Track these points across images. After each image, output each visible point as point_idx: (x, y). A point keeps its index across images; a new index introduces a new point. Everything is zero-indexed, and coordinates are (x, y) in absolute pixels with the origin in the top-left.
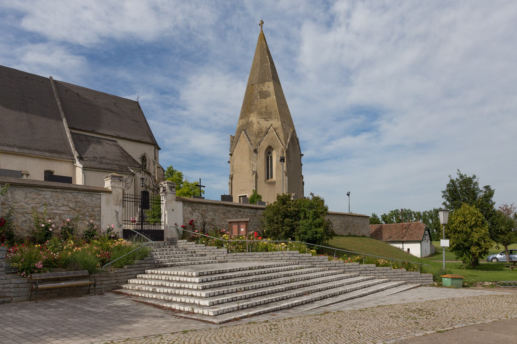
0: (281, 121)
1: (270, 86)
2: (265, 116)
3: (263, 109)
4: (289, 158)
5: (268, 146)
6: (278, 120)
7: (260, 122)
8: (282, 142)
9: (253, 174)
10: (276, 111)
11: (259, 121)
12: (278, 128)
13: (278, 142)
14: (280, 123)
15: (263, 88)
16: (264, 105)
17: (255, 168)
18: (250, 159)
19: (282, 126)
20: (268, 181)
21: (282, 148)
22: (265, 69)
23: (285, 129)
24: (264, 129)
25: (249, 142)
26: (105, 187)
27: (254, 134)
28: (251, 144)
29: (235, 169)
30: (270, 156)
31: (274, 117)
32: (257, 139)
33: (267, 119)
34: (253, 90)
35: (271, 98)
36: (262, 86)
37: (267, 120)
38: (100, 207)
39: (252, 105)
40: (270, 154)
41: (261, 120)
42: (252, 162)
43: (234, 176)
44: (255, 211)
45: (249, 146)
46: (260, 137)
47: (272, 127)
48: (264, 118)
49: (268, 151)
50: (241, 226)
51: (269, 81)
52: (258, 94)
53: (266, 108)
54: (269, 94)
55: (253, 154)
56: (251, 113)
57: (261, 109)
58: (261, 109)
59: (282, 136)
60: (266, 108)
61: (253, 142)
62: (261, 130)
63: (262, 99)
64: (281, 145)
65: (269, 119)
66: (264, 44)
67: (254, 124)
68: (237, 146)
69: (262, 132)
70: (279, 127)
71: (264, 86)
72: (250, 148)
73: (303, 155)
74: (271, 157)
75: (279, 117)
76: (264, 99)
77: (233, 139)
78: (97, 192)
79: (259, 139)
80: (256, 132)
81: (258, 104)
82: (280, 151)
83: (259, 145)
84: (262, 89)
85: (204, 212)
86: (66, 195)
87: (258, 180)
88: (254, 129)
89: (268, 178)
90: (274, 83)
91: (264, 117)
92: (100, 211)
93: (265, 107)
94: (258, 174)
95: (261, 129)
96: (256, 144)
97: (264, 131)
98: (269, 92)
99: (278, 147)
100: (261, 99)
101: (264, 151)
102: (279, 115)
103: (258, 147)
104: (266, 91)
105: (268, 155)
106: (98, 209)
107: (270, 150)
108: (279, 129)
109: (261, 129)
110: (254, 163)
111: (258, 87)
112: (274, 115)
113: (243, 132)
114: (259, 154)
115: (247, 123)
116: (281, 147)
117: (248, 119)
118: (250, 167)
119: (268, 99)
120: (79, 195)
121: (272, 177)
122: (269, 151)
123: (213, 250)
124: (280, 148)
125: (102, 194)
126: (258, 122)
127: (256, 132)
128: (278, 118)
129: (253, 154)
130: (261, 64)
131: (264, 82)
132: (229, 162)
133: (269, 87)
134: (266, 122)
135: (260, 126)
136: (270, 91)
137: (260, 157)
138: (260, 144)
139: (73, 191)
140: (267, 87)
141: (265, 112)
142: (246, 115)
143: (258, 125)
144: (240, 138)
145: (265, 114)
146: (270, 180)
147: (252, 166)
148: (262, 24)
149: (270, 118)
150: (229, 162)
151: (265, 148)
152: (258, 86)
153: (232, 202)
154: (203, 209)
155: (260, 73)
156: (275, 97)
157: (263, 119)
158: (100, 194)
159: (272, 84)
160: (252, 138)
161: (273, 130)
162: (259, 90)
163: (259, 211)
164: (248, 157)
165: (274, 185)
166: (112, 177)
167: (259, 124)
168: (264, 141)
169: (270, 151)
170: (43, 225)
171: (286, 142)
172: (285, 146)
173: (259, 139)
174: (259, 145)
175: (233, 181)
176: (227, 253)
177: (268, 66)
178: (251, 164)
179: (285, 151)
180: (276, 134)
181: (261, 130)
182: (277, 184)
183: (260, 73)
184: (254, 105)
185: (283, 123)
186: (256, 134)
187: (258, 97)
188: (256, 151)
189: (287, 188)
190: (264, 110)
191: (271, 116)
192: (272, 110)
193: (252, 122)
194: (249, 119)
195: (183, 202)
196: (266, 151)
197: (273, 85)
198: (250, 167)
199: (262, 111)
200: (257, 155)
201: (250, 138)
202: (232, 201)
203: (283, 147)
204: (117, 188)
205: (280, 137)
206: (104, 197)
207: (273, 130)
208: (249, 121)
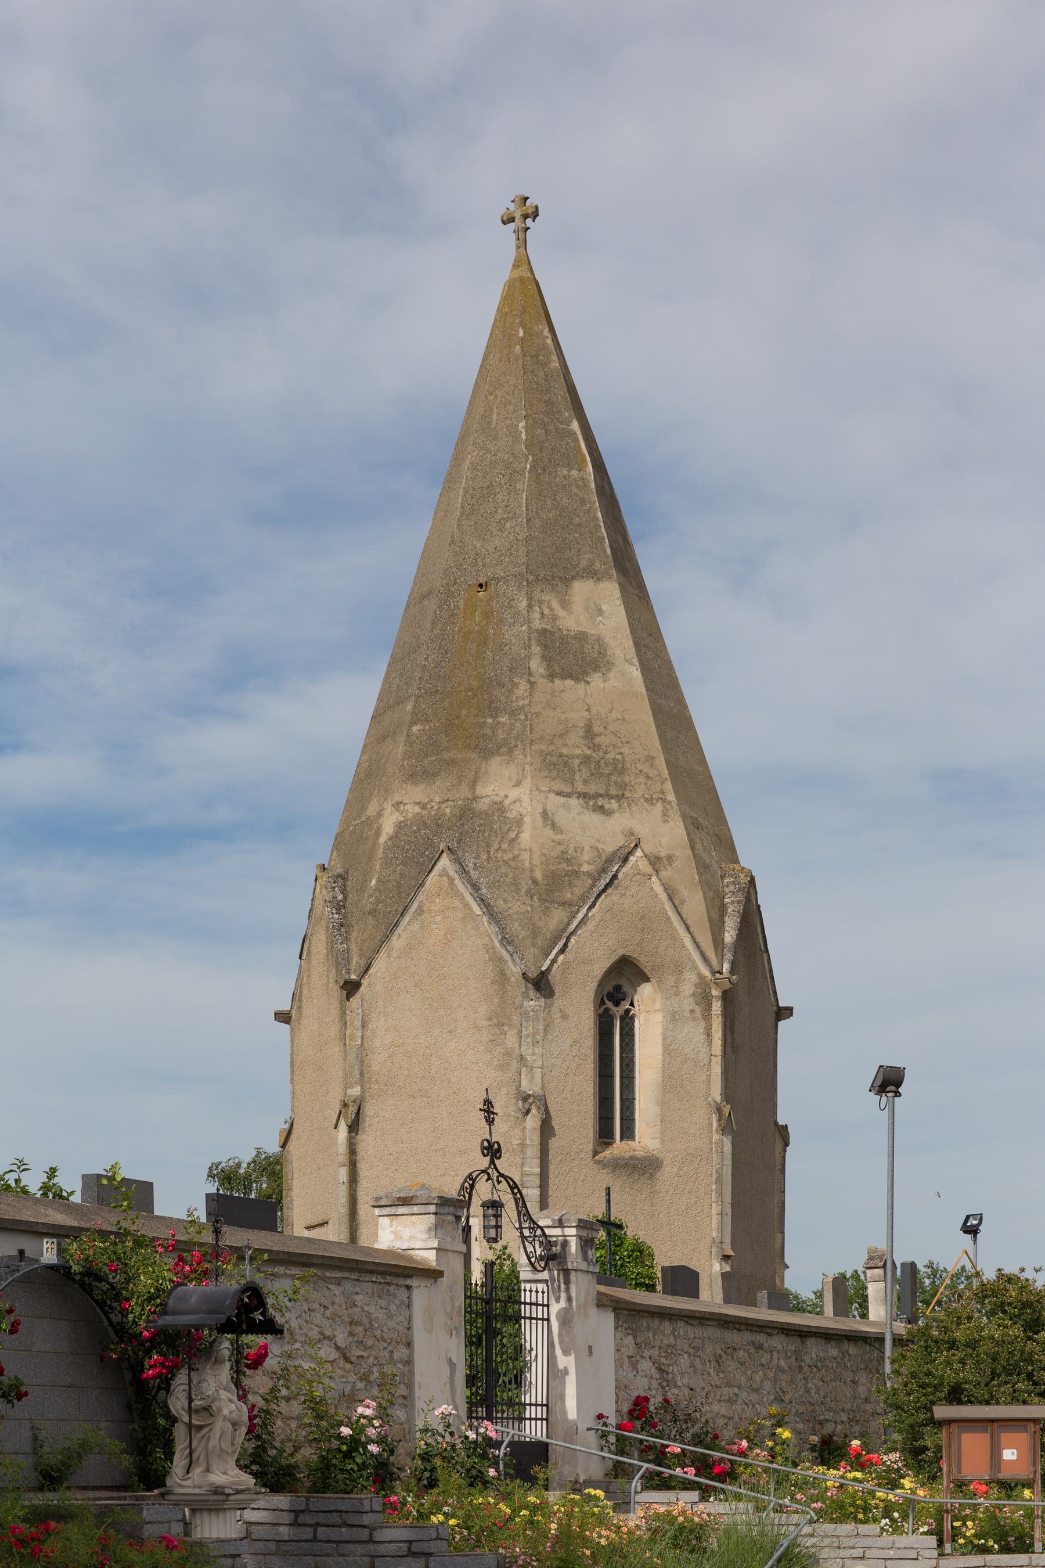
0: (683, 816)
1: (604, 607)
2: (585, 782)
3: (574, 738)
4: (732, 1033)
5: (614, 958)
6: (665, 813)
7: (562, 818)
8: (700, 939)
9: (528, 1112)
10: (651, 759)
11: (549, 807)
12: (670, 858)
13: (675, 938)
14: (683, 832)
15: (561, 613)
16: (578, 717)
17: (538, 1079)
18: (499, 1021)
19: (693, 849)
20: (607, 1153)
21: (701, 977)
22: (565, 502)
23: (707, 867)
24: (586, 856)
25: (492, 929)
26: (376, 1246)
27: (525, 883)
28: (506, 940)
29: (375, 1068)
30: (618, 1011)
31: (640, 790)
32: (546, 911)
33: (600, 802)
34: (487, 615)
35: (614, 680)
36: (555, 604)
37: (601, 809)
38: (409, 1345)
39: (494, 711)
40: (617, 1004)
41: (567, 808)
42: (511, 1041)
43: (369, 1110)
44: (792, 1344)
45: (489, 949)
46: (564, 904)
47: (639, 853)
48: (583, 795)
49: (609, 988)
50: (1005, 1437)
51: (592, 574)
52: (536, 649)
53: (589, 734)
54: (602, 653)
55: (525, 995)
56: (487, 754)
57: (558, 741)
58: (558, 741)
59: (695, 903)
60: (589, 734)
61: (516, 928)
62: (568, 861)
63: (558, 682)
64: (696, 956)
65: (614, 804)
66: (544, 344)
67: (519, 822)
68: (397, 942)
69: (576, 873)
70: (677, 853)
71: (565, 604)
72: (501, 959)
73: (788, 1012)
74: (628, 1020)
75: (671, 797)
76: (569, 682)
77: (344, 892)
78: (398, 1275)
79: (558, 916)
80: (538, 875)
81: (538, 709)
82: (688, 989)
83: (562, 951)
84: (555, 618)
85: (666, 1358)
86: (327, 1293)
87: (553, 1143)
88: (526, 856)
89: (604, 1135)
90: (623, 588)
91: (580, 787)
92: (409, 1362)
93: (581, 733)
94: (553, 1114)
95: (564, 857)
96: (539, 942)
97: (585, 868)
98: (599, 640)
99: (679, 969)
100: (551, 677)
101: (592, 986)
102: (668, 785)
103: (554, 961)
104: (582, 637)
105: (609, 1004)
106: (401, 1353)
107: (623, 982)
108: (676, 864)
109: (564, 857)
110: (526, 1050)
111: (530, 606)
112: (642, 779)
113: (445, 862)
114: (558, 1002)
115: (466, 812)
116: (695, 967)
117: (473, 785)
118: (502, 1067)
119: (596, 680)
120: (358, 1290)
121: (628, 1133)
122: (614, 983)
123: (861, 1542)
124: (690, 977)
125: (414, 1282)
126: (545, 815)
127: (538, 875)
128: (664, 801)
129: (525, 995)
130: (539, 469)
131: (567, 581)
132: (283, 1017)
133: (600, 612)
134: (595, 819)
135: (557, 837)
136: (608, 640)
137: (565, 1017)
138: (566, 945)
139: (346, 1275)
140: (587, 609)
141: (586, 760)
142: (453, 762)
143: (548, 832)
144: (421, 896)
145: (585, 773)
146: (619, 1147)
147: (515, 1065)
148: (525, 217)
149: (620, 798)
150: (283, 1017)
151: (601, 967)
152: (530, 599)
153: (697, 1297)
154: (666, 1342)
155: (537, 523)
156: (636, 673)
157: (574, 802)
158: (408, 1282)
159: (617, 594)
160: (514, 906)
161: (649, 869)
162: (538, 624)
163: (811, 1342)
164: (483, 1009)
165: (652, 1175)
166: (583, 1228)
167: (553, 825)
168: (590, 926)
169: (618, 988)
170: (346, 1431)
171: (718, 943)
172: (717, 968)
173: (558, 916)
174: (562, 951)
175: (367, 1142)
176: (935, 1553)
177: (586, 486)
178: (508, 1054)
179: (716, 992)
180: (663, 896)
181: (568, 861)
182: (667, 1173)
183: (537, 523)
184: (512, 713)
185: (693, 826)
186: (535, 882)
187: (536, 665)
188: (541, 984)
189: (728, 1199)
190: (575, 746)
191: (623, 786)
192: (626, 750)
193: (500, 808)
194: (480, 790)
195: (614, 1310)
196: (601, 985)
197: (619, 602)
198: (502, 1067)
199: (565, 751)
200: (548, 1008)
201: (500, 905)
202: (695, 1295)
203: (706, 973)
204: (450, 1254)
205: (685, 911)
206: (421, 1294)
207: (645, 867)
208: (475, 798)
